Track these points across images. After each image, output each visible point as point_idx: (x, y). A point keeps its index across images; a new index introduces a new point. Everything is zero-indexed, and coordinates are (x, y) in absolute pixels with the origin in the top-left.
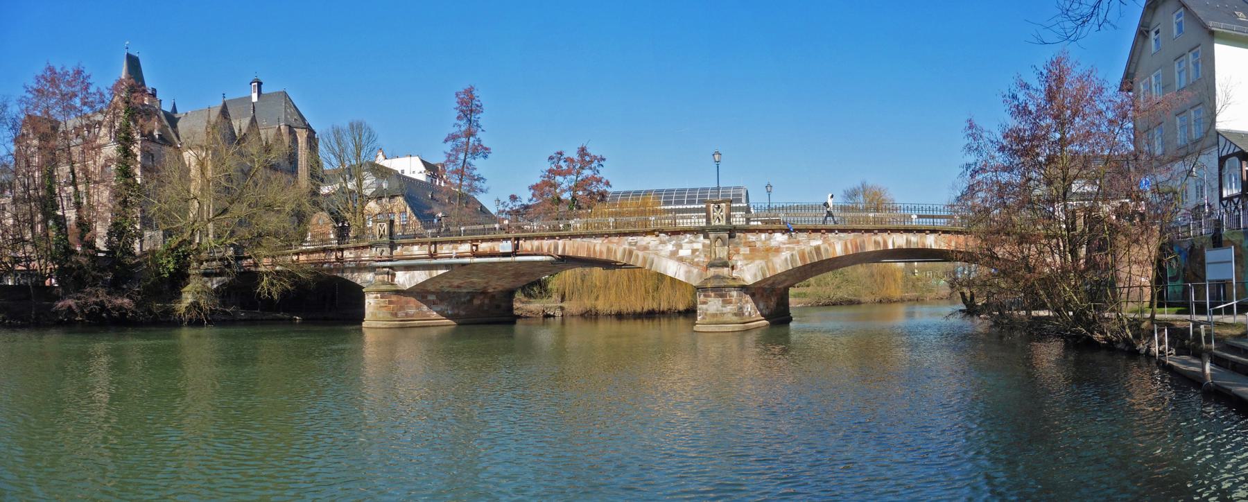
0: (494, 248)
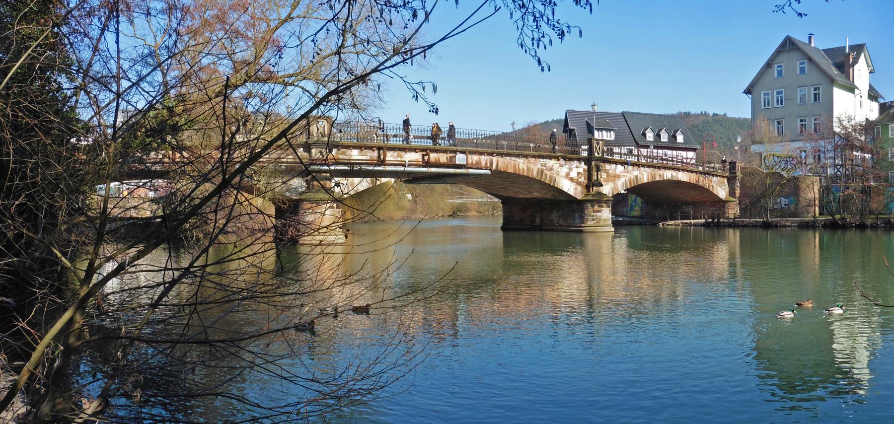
0: (439, 159)
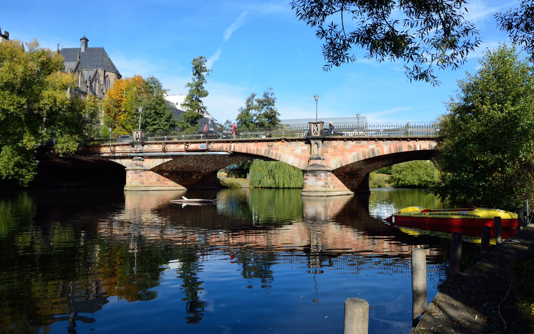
0: (198, 147)
